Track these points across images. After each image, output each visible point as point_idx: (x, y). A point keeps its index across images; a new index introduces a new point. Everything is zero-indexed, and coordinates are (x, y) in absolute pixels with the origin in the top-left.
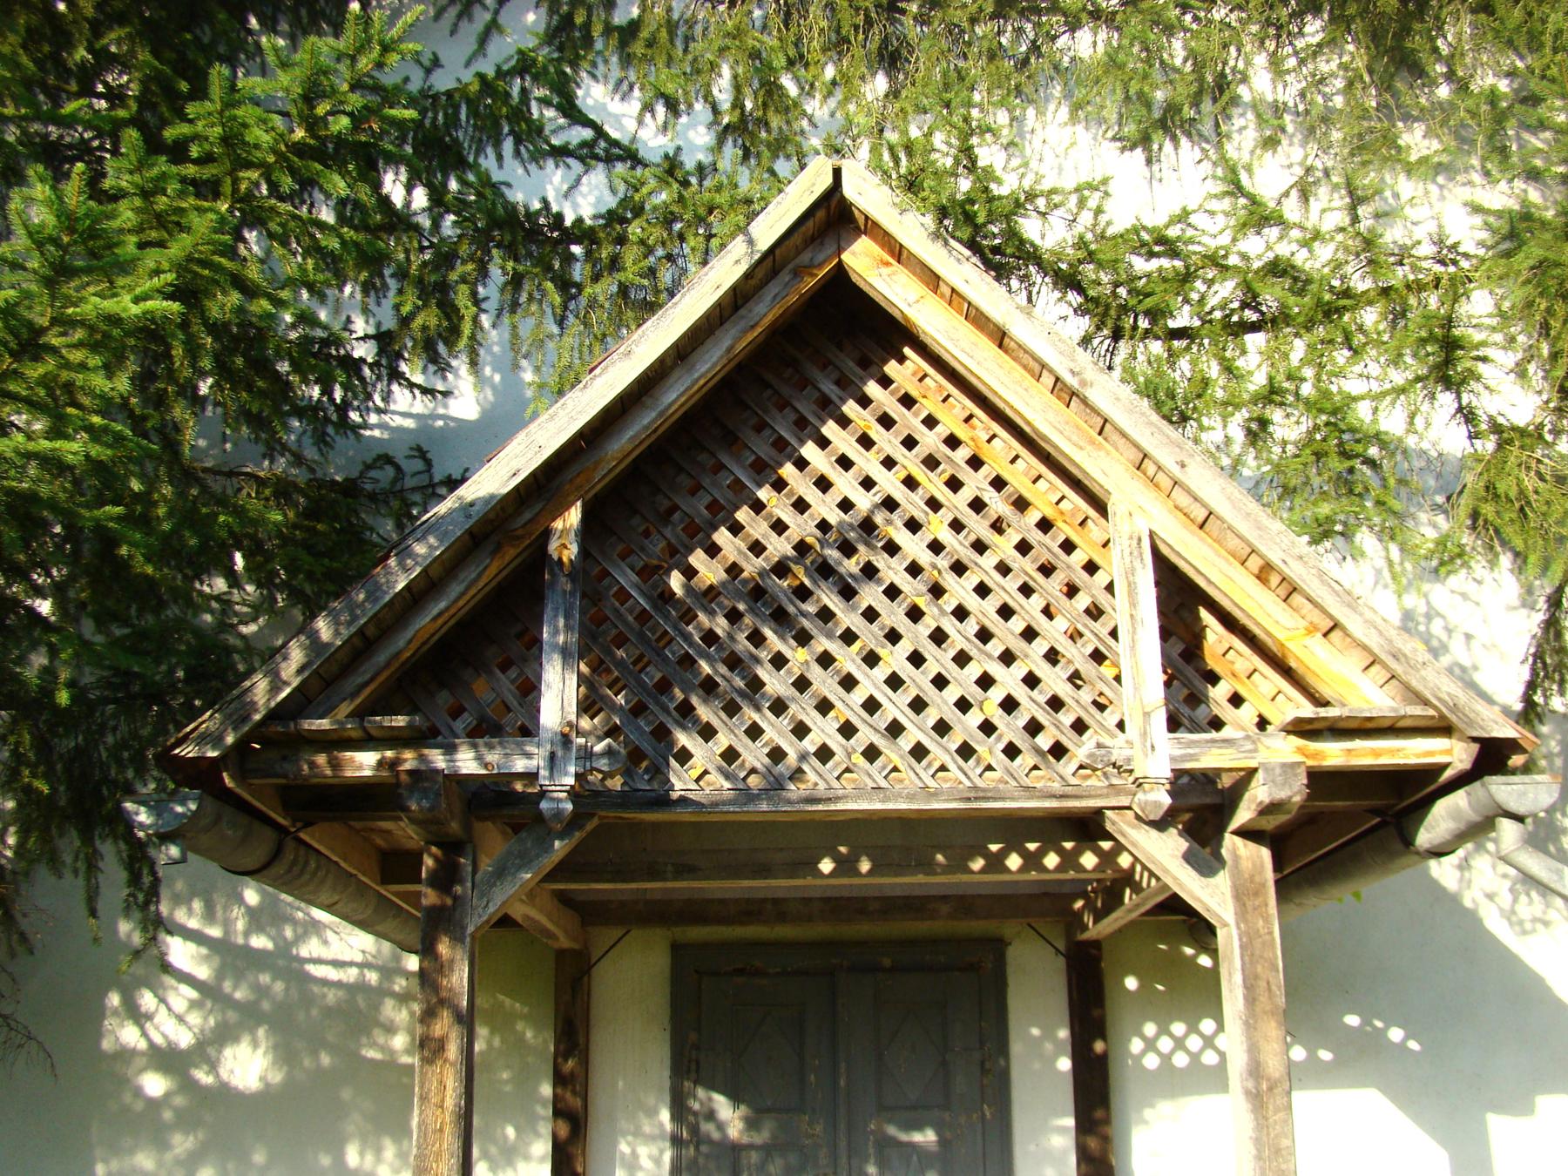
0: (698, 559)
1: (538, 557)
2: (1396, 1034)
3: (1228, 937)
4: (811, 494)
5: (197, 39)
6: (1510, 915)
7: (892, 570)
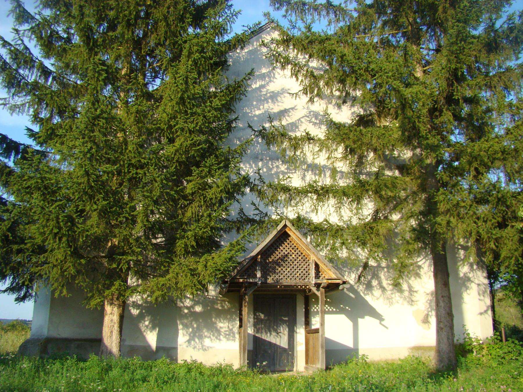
0: (269, 259)
1: (256, 260)
3: (320, 298)
4: (281, 252)
5: (72, 28)
6: (364, 293)
7: (289, 260)
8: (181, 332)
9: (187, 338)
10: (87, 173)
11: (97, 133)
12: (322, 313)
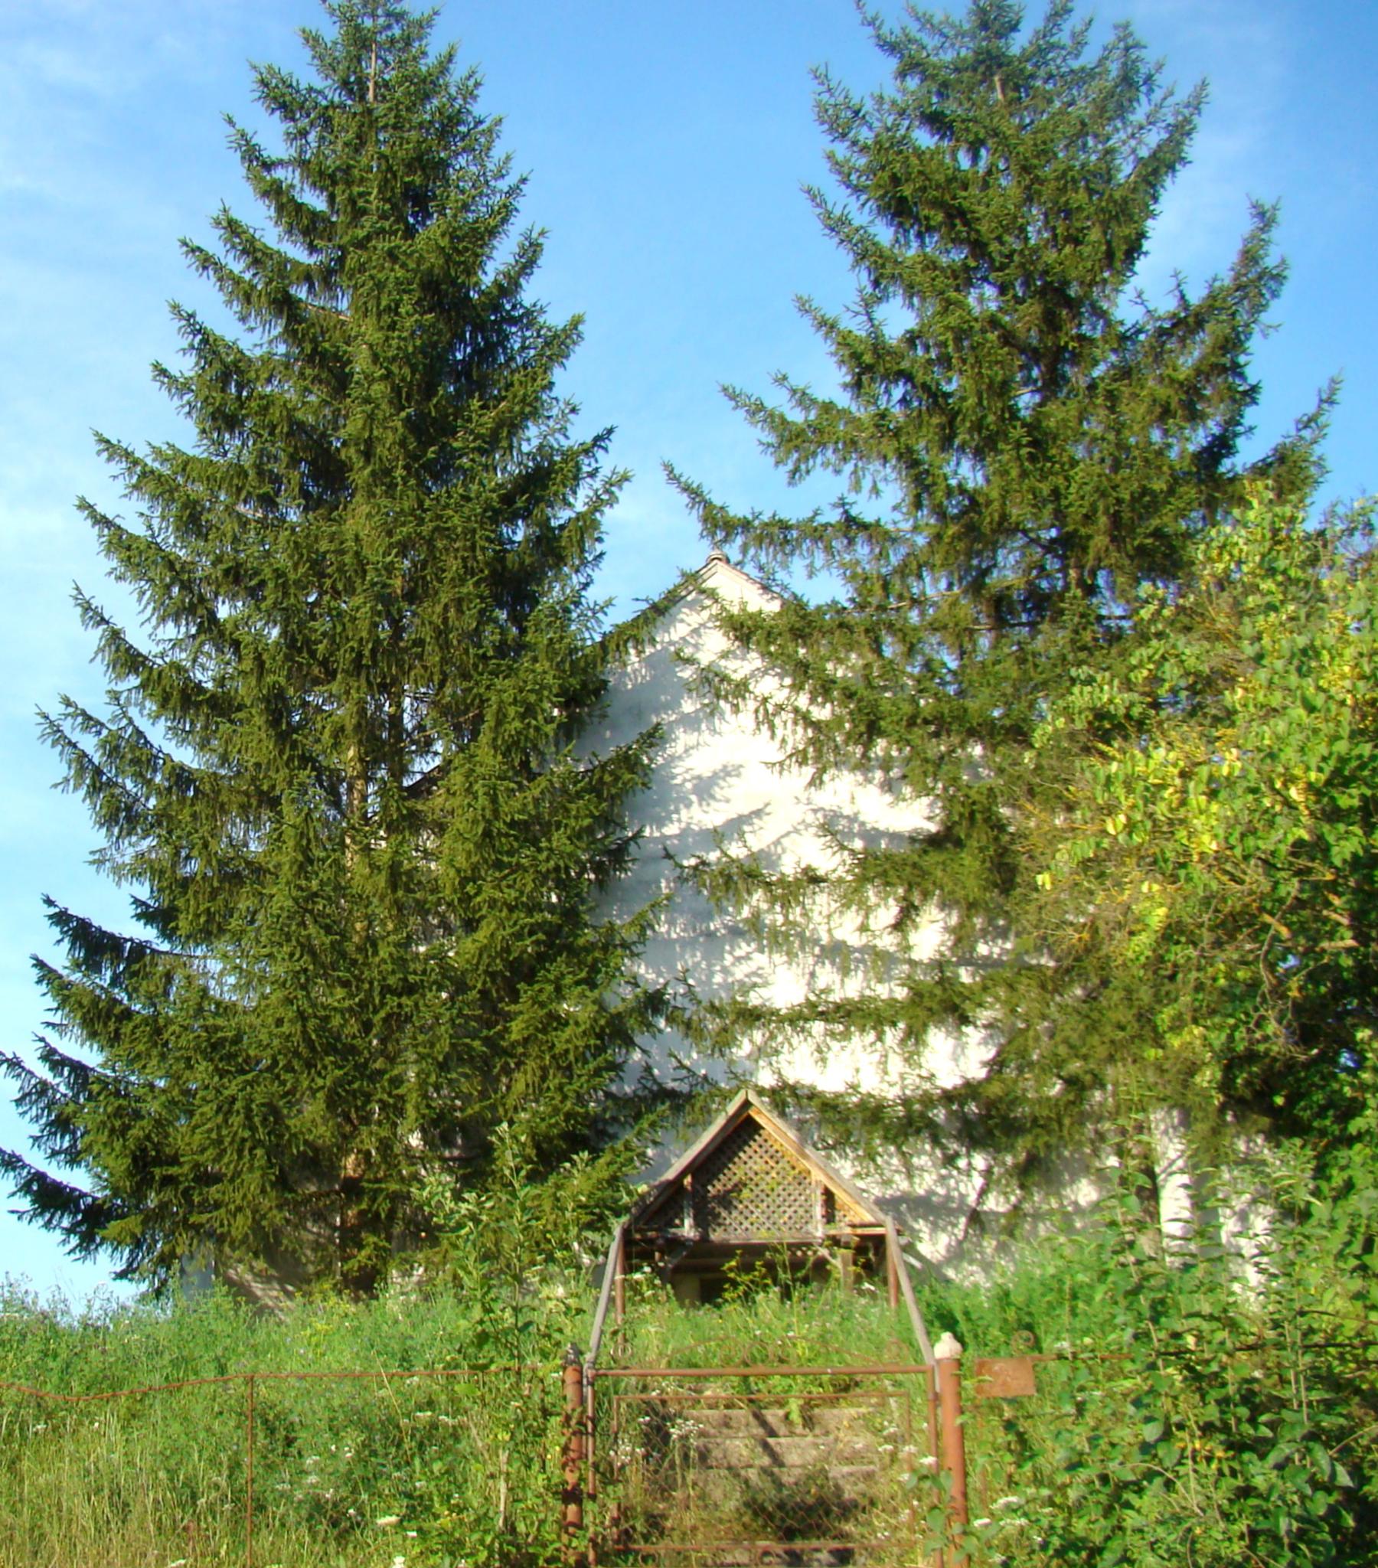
10: (302, 1016)
11: (312, 929)
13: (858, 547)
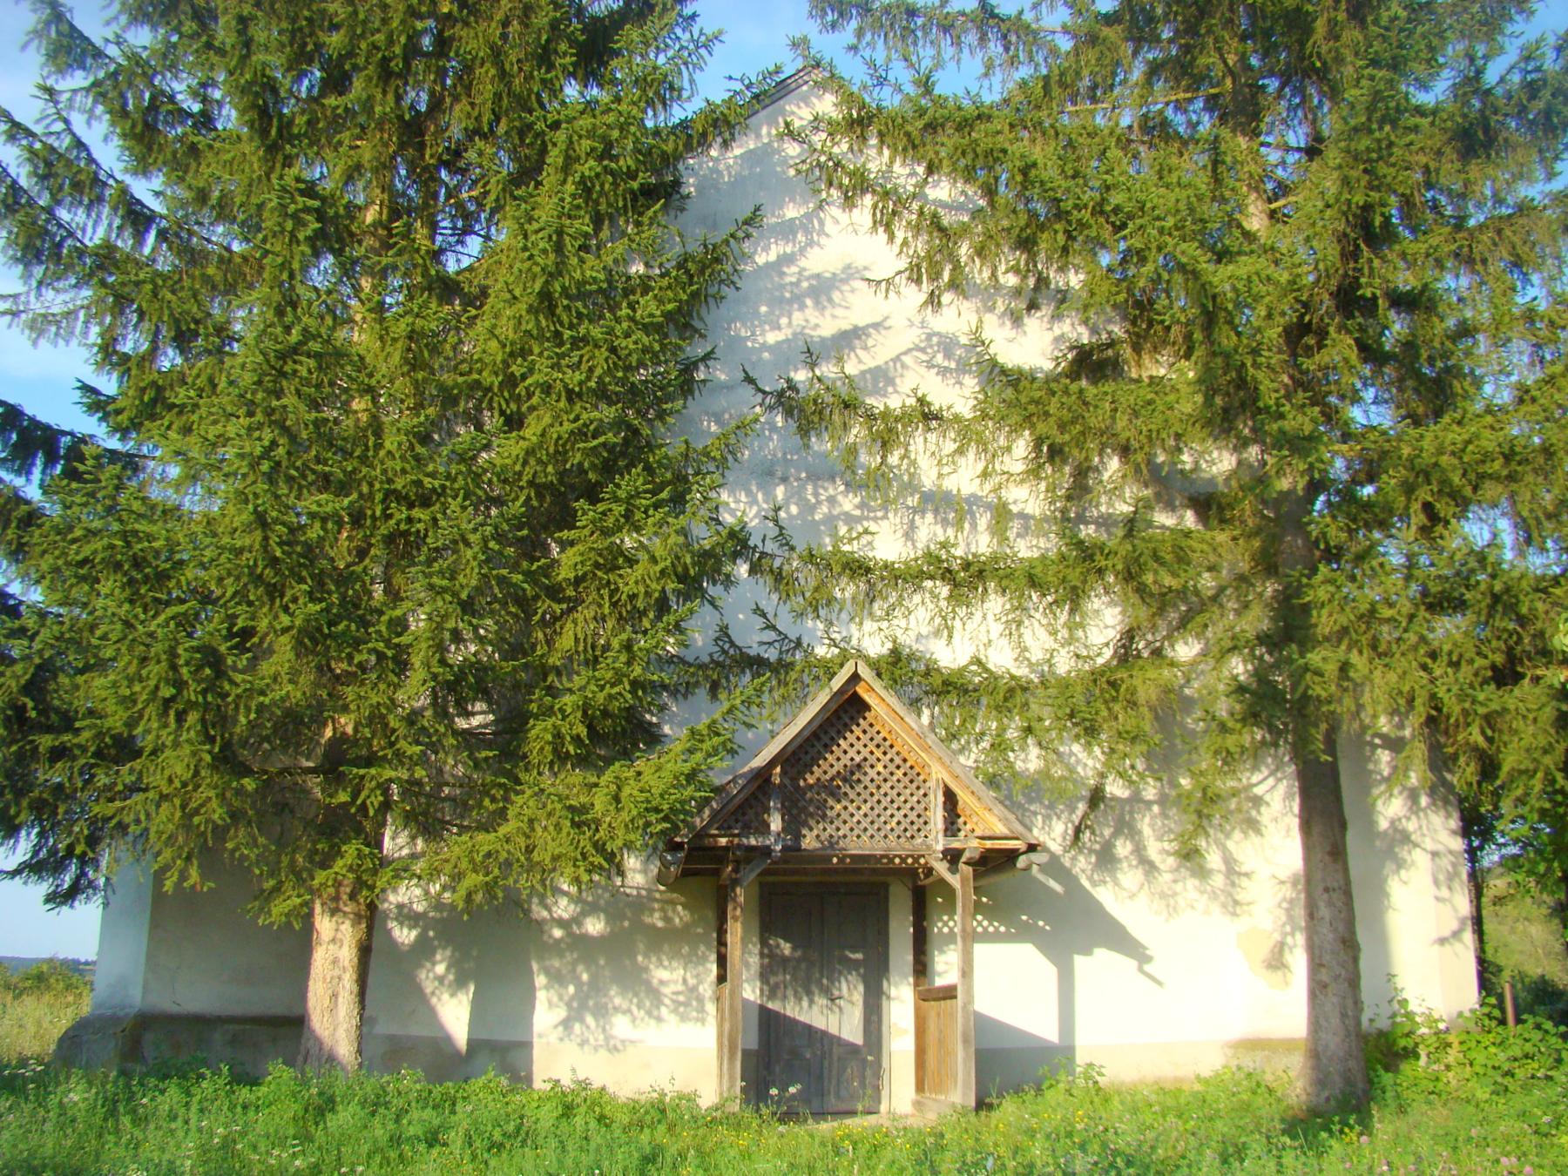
0: (808, 776)
1: (768, 780)
2: (1041, 923)
3: (959, 893)
4: (842, 755)
6: (1090, 879)
8: (541, 996)
9: (562, 1013)
11: (289, 400)
12: (964, 939)
13: (992, 45)
